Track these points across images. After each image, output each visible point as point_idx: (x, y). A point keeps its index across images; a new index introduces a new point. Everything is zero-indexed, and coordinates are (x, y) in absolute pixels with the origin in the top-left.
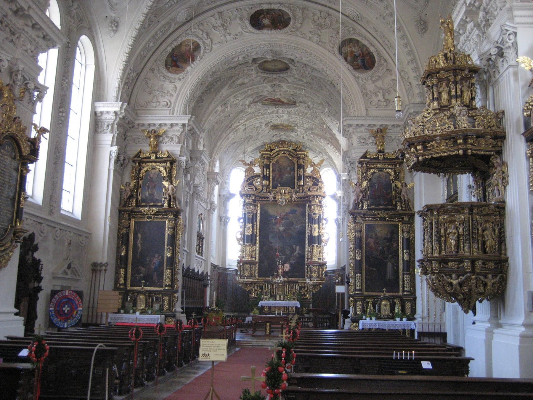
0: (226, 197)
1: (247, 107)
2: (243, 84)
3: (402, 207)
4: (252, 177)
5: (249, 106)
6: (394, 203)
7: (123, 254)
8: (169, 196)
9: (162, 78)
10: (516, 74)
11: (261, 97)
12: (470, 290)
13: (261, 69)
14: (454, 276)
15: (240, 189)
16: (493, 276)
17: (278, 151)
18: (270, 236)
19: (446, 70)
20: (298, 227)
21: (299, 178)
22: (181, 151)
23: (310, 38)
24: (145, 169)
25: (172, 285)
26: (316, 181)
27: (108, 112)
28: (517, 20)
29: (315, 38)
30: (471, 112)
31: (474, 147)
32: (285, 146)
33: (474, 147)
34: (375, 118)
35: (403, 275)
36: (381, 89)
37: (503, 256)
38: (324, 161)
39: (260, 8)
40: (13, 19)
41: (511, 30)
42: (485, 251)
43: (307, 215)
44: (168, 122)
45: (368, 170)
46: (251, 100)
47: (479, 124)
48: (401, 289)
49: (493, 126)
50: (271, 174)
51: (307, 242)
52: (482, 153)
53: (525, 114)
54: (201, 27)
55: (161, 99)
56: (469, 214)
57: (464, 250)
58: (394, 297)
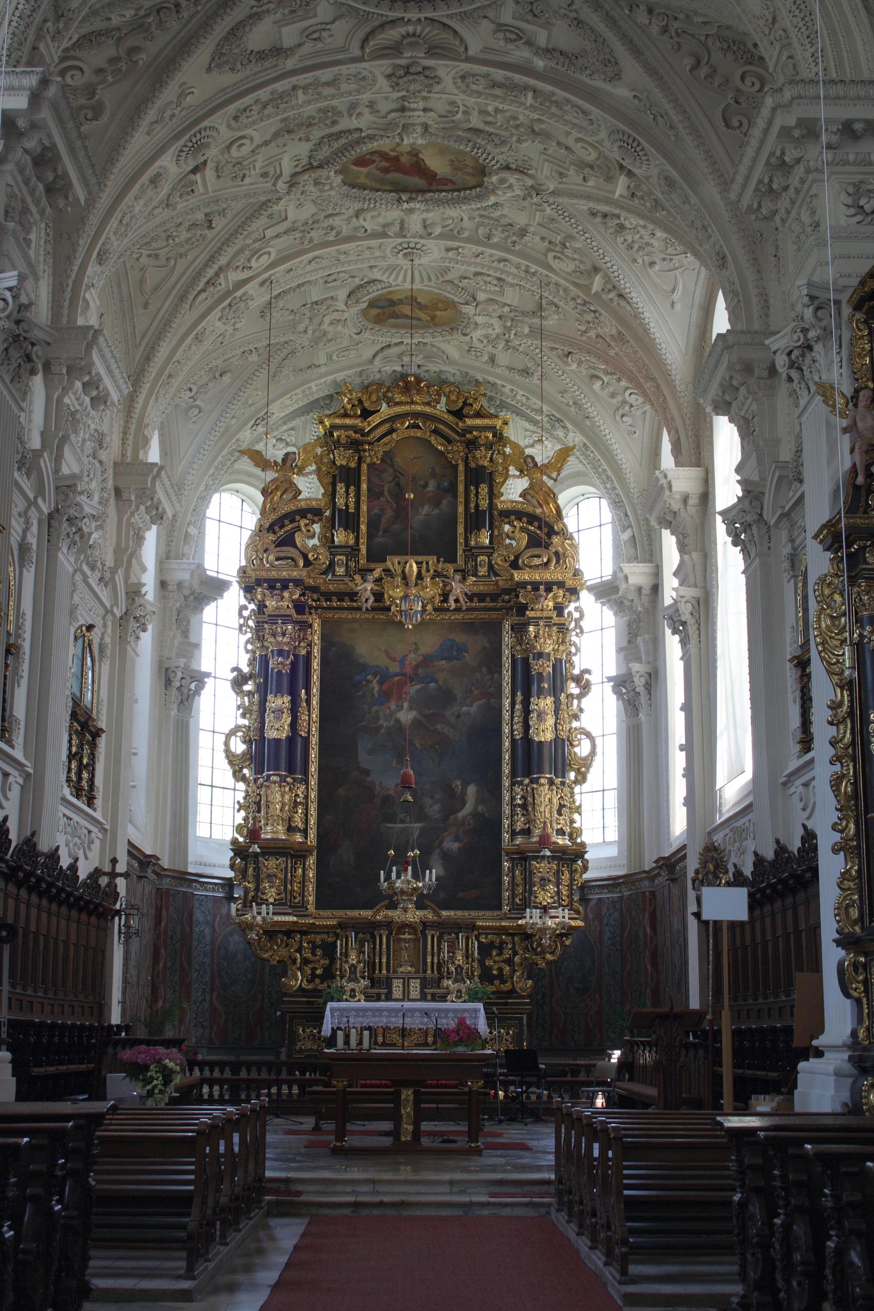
0: (187, 592)
1: (281, 186)
4: (291, 516)
11: (343, 141)
17: (393, 419)
18: (364, 745)
20: (473, 709)
21: (475, 522)
32: (416, 398)
38: (571, 460)
43: (507, 664)
46: (303, 149)
50: (364, 508)
51: (506, 770)
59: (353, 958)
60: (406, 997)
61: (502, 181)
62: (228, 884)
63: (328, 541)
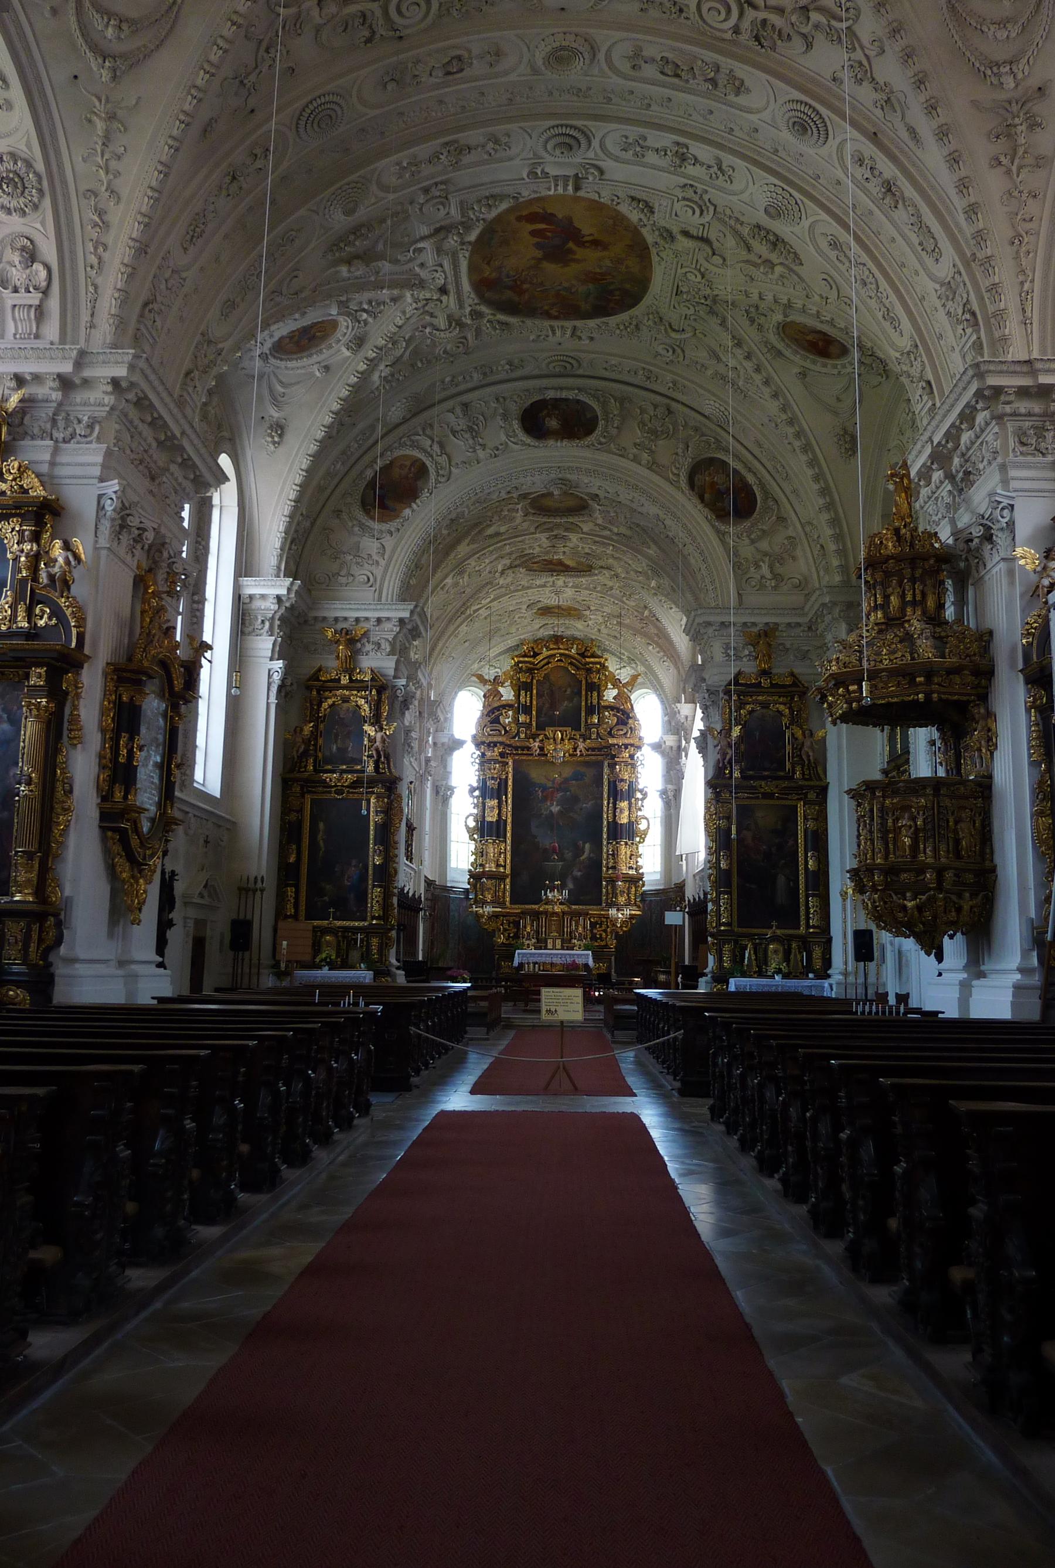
2: (498, 534)
3: (803, 774)
4: (498, 709)
5: (502, 573)
6: (788, 766)
7: (292, 859)
8: (377, 750)
9: (356, 529)
10: (1011, 573)
12: (935, 917)
13: (533, 508)
14: (908, 894)
15: (474, 732)
16: (971, 895)
19: (897, 558)
20: (588, 805)
21: (591, 711)
22: (396, 669)
23: (635, 456)
24: (330, 701)
25: (385, 917)
26: (624, 716)
27: (263, 597)
28: (1014, 484)
29: (645, 457)
30: (938, 630)
31: (942, 690)
33: (942, 690)
34: (755, 611)
35: (807, 896)
36: (766, 554)
37: (987, 863)
39: (541, 398)
40: (155, 456)
41: (1006, 502)
42: (958, 855)
43: (606, 783)
44: (373, 615)
45: (741, 705)
46: (507, 562)
47: (951, 652)
48: (803, 922)
49: (975, 655)
50: (534, 703)
52: (956, 697)
53: (1024, 641)
54: (428, 432)
55: (355, 570)
56: (934, 796)
57: (925, 853)
58: (791, 938)
59: (528, 929)
60: (554, 948)
61: (600, 573)
62: (467, 891)
63: (516, 720)
